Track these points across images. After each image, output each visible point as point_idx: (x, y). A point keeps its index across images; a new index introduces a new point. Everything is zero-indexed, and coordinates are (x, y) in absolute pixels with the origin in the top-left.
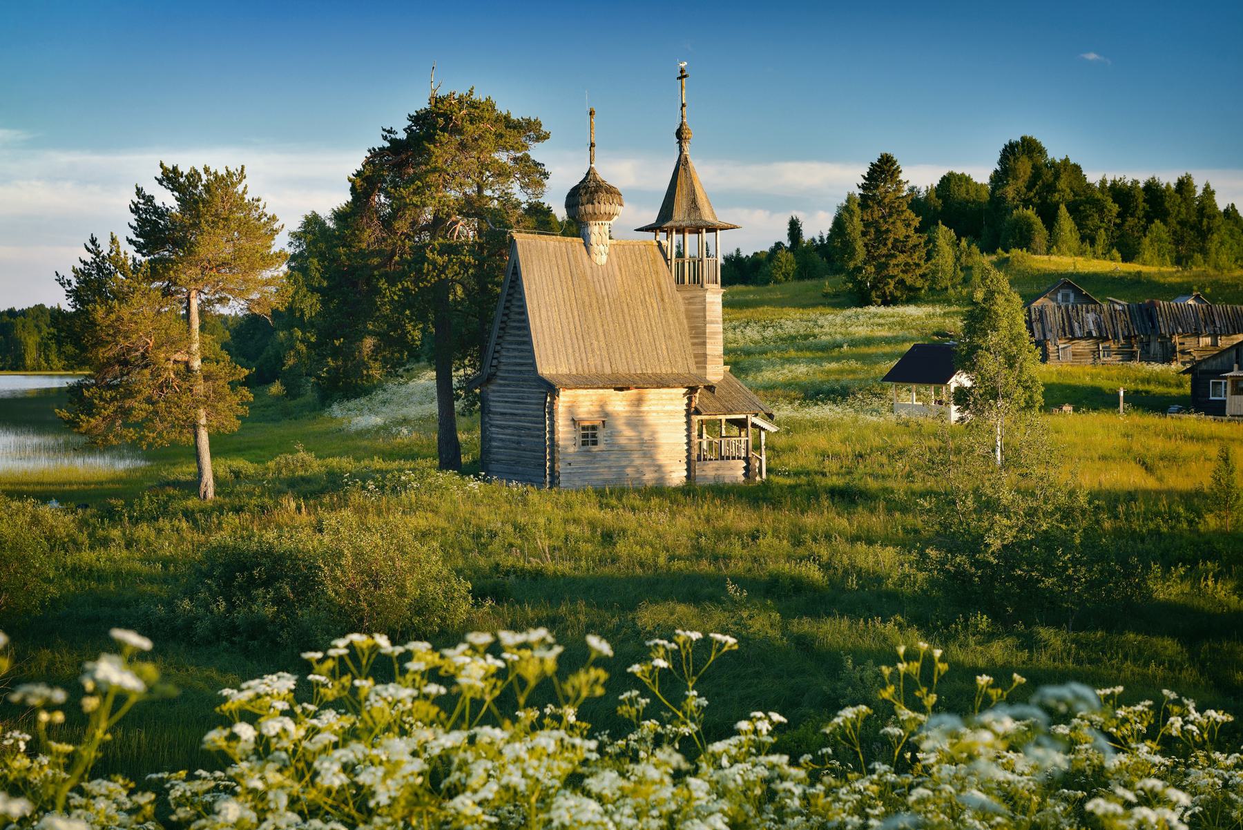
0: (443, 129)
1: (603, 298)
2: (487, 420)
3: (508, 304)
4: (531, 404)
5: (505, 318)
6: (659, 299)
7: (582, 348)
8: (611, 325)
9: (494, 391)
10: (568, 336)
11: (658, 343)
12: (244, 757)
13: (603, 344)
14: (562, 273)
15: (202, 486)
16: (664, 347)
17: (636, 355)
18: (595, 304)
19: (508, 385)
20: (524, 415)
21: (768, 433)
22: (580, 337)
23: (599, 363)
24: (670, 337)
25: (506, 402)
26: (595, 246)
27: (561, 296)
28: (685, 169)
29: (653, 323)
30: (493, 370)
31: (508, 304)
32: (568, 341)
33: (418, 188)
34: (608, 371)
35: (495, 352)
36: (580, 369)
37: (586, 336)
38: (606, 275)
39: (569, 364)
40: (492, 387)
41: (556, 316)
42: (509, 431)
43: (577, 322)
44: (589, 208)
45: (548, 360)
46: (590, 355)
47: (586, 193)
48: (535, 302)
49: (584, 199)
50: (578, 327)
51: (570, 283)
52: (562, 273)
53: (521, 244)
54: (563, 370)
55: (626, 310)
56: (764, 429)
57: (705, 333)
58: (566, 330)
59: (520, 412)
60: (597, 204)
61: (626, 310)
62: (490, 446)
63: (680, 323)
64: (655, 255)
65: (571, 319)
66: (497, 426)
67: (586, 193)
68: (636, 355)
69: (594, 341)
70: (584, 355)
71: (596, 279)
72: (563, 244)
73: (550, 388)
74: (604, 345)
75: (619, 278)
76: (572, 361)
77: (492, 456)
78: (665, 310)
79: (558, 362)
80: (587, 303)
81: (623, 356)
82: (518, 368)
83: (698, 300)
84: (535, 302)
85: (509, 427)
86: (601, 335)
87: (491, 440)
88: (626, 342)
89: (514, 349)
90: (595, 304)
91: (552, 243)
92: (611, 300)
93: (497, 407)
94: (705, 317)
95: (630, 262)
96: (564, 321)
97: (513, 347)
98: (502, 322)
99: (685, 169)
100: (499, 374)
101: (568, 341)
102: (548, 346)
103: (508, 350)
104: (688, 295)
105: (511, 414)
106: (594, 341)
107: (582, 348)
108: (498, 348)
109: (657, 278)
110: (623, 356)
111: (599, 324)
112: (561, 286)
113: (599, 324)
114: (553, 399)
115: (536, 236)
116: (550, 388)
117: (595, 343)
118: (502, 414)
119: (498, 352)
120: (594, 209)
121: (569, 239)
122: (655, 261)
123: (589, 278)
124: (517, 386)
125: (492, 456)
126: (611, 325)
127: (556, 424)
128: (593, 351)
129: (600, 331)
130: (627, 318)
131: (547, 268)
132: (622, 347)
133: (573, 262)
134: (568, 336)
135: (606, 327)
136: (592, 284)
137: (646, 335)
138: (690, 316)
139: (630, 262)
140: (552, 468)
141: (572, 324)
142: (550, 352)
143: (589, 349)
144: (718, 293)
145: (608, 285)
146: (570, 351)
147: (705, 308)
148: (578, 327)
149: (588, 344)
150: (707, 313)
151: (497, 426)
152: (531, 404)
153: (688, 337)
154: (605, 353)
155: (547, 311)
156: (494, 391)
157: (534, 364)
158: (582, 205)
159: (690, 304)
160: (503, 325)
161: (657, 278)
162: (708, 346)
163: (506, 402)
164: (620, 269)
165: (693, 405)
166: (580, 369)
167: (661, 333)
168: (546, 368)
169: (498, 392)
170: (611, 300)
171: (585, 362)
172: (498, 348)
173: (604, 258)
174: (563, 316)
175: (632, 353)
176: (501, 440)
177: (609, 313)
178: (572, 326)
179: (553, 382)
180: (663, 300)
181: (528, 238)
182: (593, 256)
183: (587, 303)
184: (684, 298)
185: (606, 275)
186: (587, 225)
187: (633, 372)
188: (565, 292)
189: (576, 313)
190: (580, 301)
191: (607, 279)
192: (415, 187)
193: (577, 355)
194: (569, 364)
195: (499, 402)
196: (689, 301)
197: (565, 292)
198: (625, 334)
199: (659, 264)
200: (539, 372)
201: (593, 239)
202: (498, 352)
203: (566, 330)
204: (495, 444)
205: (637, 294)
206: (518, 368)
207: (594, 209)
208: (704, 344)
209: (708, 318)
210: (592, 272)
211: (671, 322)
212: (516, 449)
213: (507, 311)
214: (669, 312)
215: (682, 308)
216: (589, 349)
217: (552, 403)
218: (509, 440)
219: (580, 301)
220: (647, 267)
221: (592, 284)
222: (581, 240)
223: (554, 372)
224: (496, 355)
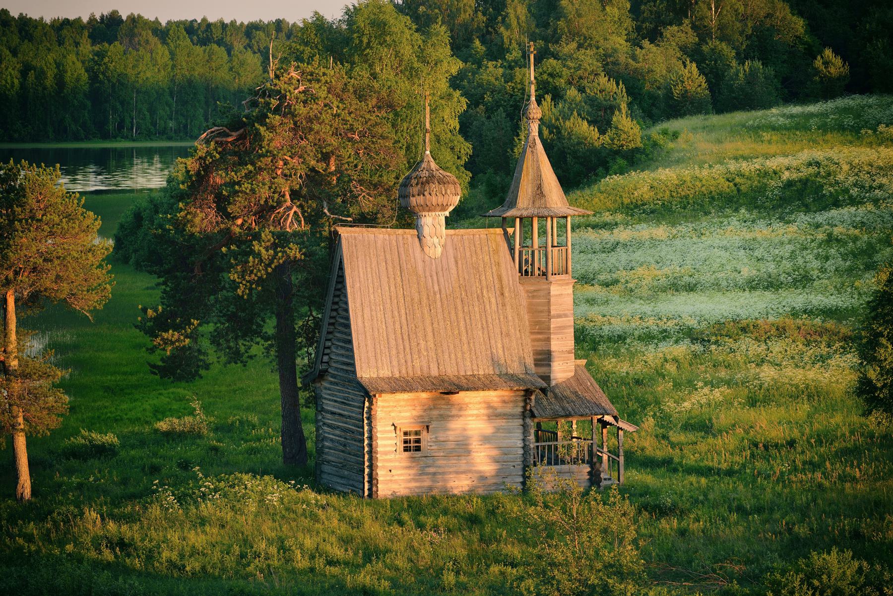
0: (277, 111)
1: (435, 293)
2: (320, 417)
3: (336, 300)
4: (354, 406)
5: (334, 314)
6: (498, 293)
7: (408, 350)
8: (442, 323)
9: (326, 388)
10: (392, 336)
11: (493, 342)
12: (773, 452)
13: (431, 344)
14: (390, 269)
15: (19, 487)
16: (500, 346)
17: (467, 355)
18: (425, 301)
19: (337, 384)
20: (350, 417)
21: (625, 432)
22: (406, 337)
23: (425, 365)
24: (508, 335)
25: (336, 401)
26: (428, 238)
27: (387, 293)
28: (532, 152)
29: (490, 320)
30: (324, 367)
31: (336, 300)
32: (393, 343)
33: (251, 172)
34: (434, 372)
35: (325, 348)
36: (404, 371)
37: (412, 336)
38: (439, 269)
39: (392, 366)
40: (325, 384)
41: (380, 315)
42: (337, 432)
43: (404, 321)
44: (420, 200)
45: (368, 363)
46: (415, 356)
47: (417, 184)
48: (358, 301)
49: (415, 190)
50: (405, 327)
51: (399, 279)
52: (390, 269)
53: (347, 239)
54: (385, 373)
55: (460, 307)
56: (621, 429)
57: (549, 329)
58: (390, 330)
59: (346, 413)
60: (428, 196)
61: (460, 307)
62: (323, 446)
63: (520, 319)
64: (497, 245)
65: (397, 318)
66: (329, 426)
67: (417, 184)
68: (467, 355)
69: (421, 342)
70: (409, 357)
71: (428, 274)
72: (393, 238)
73: (366, 394)
74: (432, 346)
75: (454, 271)
76: (395, 363)
77: (325, 456)
78: (504, 305)
79: (380, 365)
80: (416, 300)
81: (453, 356)
82: (345, 367)
83: (542, 293)
84: (358, 301)
85: (338, 427)
86: (430, 334)
87: (324, 439)
88: (457, 342)
89: (342, 347)
90: (425, 301)
91: (379, 236)
92: (444, 296)
93: (329, 406)
94: (550, 312)
95: (468, 254)
96: (390, 321)
97: (341, 344)
98: (331, 317)
99: (532, 152)
100: (330, 370)
101: (393, 343)
102: (370, 347)
103: (337, 347)
104: (532, 288)
105: (340, 415)
106: (421, 342)
107: (408, 350)
108: (328, 344)
109: (498, 270)
110: (453, 356)
111: (428, 322)
112: (389, 282)
113: (428, 322)
114: (371, 403)
115: (364, 229)
116: (366, 394)
117: (422, 343)
118: (333, 413)
119: (329, 348)
120: (425, 200)
121: (400, 231)
122: (496, 251)
123: (421, 272)
124: (344, 386)
125: (325, 456)
126: (442, 323)
127: (374, 430)
128: (419, 351)
129: (429, 330)
130: (461, 315)
131: (374, 264)
132: (452, 347)
133: (403, 257)
134: (392, 336)
135: (435, 325)
136: (423, 279)
137: (480, 333)
138: (532, 310)
139: (468, 254)
140: (370, 475)
141: (398, 323)
142: (371, 354)
143: (415, 350)
144: (567, 284)
145: (442, 280)
146: (394, 352)
147: (549, 302)
148: (405, 327)
149: (414, 344)
150: (552, 308)
151: (329, 426)
152: (354, 406)
153: (528, 334)
154: (432, 354)
155: (371, 310)
156: (326, 388)
157: (354, 372)
158: (413, 196)
159: (533, 297)
160: (332, 321)
161: (498, 270)
162: (553, 343)
163: (336, 401)
164: (456, 262)
165: (528, 407)
166: (404, 371)
167: (498, 331)
168: (365, 372)
169: (329, 389)
170: (444, 296)
171: (409, 364)
172: (328, 344)
173: (439, 250)
174: (389, 315)
175: (463, 353)
176: (332, 440)
177: (440, 311)
178: (398, 326)
179: (369, 388)
180: (502, 294)
181: (355, 232)
182: (426, 249)
183: (416, 300)
184: (527, 291)
185: (439, 269)
186: (419, 217)
187: (462, 373)
188: (393, 289)
189: (403, 312)
190: (408, 299)
191: (440, 274)
192: (246, 171)
193: (401, 356)
194: (392, 366)
195: (330, 400)
196: (532, 295)
197: (393, 289)
198: (456, 332)
199: (501, 254)
200: (359, 375)
201: (426, 231)
202: (329, 348)
203: (390, 330)
204: (327, 444)
205: (474, 288)
206: (345, 367)
207: (425, 200)
208: (548, 340)
209: (552, 313)
210: (424, 267)
211: (510, 318)
212: (343, 451)
213: (336, 307)
214: (508, 307)
215: (524, 303)
216: (415, 350)
217: (370, 409)
218: (338, 442)
219: (408, 299)
220: (487, 258)
221: (423, 279)
222: (415, 232)
223: (375, 376)
224: (327, 351)
